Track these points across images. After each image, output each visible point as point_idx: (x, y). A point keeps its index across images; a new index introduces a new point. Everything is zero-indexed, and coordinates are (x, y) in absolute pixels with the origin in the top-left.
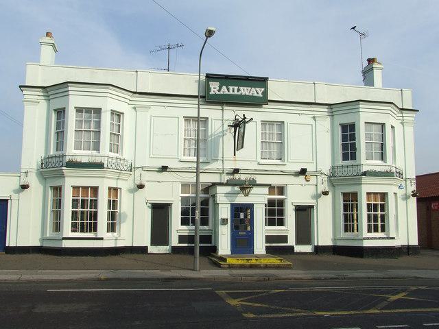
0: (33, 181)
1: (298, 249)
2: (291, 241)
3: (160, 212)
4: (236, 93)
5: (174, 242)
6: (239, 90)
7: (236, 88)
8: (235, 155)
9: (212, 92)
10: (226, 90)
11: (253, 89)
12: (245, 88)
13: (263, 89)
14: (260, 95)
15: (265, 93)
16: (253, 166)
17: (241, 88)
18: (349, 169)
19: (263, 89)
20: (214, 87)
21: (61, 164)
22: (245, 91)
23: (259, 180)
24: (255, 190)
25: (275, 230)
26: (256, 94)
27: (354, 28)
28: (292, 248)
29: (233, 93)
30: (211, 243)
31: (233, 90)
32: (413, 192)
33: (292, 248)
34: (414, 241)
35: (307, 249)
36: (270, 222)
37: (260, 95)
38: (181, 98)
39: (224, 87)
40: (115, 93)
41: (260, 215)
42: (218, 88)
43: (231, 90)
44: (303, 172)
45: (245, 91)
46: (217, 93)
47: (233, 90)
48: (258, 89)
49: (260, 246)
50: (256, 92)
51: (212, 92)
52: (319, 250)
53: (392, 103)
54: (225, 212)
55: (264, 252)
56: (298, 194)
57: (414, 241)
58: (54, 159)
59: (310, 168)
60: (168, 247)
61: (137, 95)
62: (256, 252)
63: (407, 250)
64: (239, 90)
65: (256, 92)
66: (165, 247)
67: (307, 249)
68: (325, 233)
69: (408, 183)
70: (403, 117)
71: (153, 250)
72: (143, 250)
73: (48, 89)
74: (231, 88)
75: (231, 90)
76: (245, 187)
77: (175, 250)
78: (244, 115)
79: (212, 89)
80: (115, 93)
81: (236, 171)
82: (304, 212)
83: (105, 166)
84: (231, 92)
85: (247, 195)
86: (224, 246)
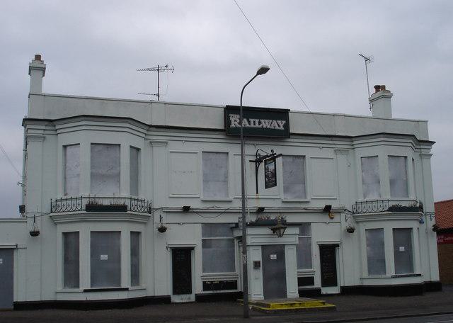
0: (43, 225)
1: (325, 291)
2: (318, 283)
3: (181, 257)
4: (257, 125)
5: (197, 288)
6: (260, 123)
7: (257, 121)
8: (257, 193)
9: (233, 126)
10: (247, 123)
11: (274, 121)
12: (266, 121)
13: (284, 122)
14: (282, 128)
15: (287, 126)
16: (277, 205)
17: (262, 121)
18: (384, 204)
19: (284, 122)
20: (235, 120)
21: (79, 208)
22: (266, 124)
23: (290, 219)
24: (288, 231)
25: (306, 272)
26: (277, 127)
27: (367, 59)
28: (319, 290)
29: (255, 126)
30: (236, 288)
31: (254, 123)
32: (434, 226)
33: (319, 290)
34: (435, 277)
35: (334, 290)
36: (300, 265)
37: (282, 128)
38: (182, 131)
39: (245, 120)
40: (133, 127)
41: (291, 257)
42: (238, 121)
43: (252, 123)
44: (328, 209)
45: (266, 124)
46: (238, 125)
47: (254, 123)
48: (279, 122)
49: (292, 289)
50: (278, 125)
51: (233, 126)
52: (346, 291)
53: (413, 136)
54: (255, 255)
55: (297, 295)
56: (323, 233)
57: (194, 300)
58: (74, 202)
59: (335, 205)
60: (320, 286)
61: (154, 129)
62: (289, 295)
63: (430, 287)
64: (260, 123)
65: (278, 125)
66: (188, 296)
67: (334, 290)
68: (352, 271)
69: (428, 217)
70: (56, 130)
71: (176, 299)
72: (165, 300)
73: (353, 139)
74: (252, 120)
75: (252, 123)
76: (278, 226)
77: (200, 298)
78: (272, 151)
79: (233, 122)
80: (133, 127)
81: (261, 210)
82: (329, 253)
83: (129, 208)
84: (252, 125)
85: (281, 236)
86: (256, 291)
